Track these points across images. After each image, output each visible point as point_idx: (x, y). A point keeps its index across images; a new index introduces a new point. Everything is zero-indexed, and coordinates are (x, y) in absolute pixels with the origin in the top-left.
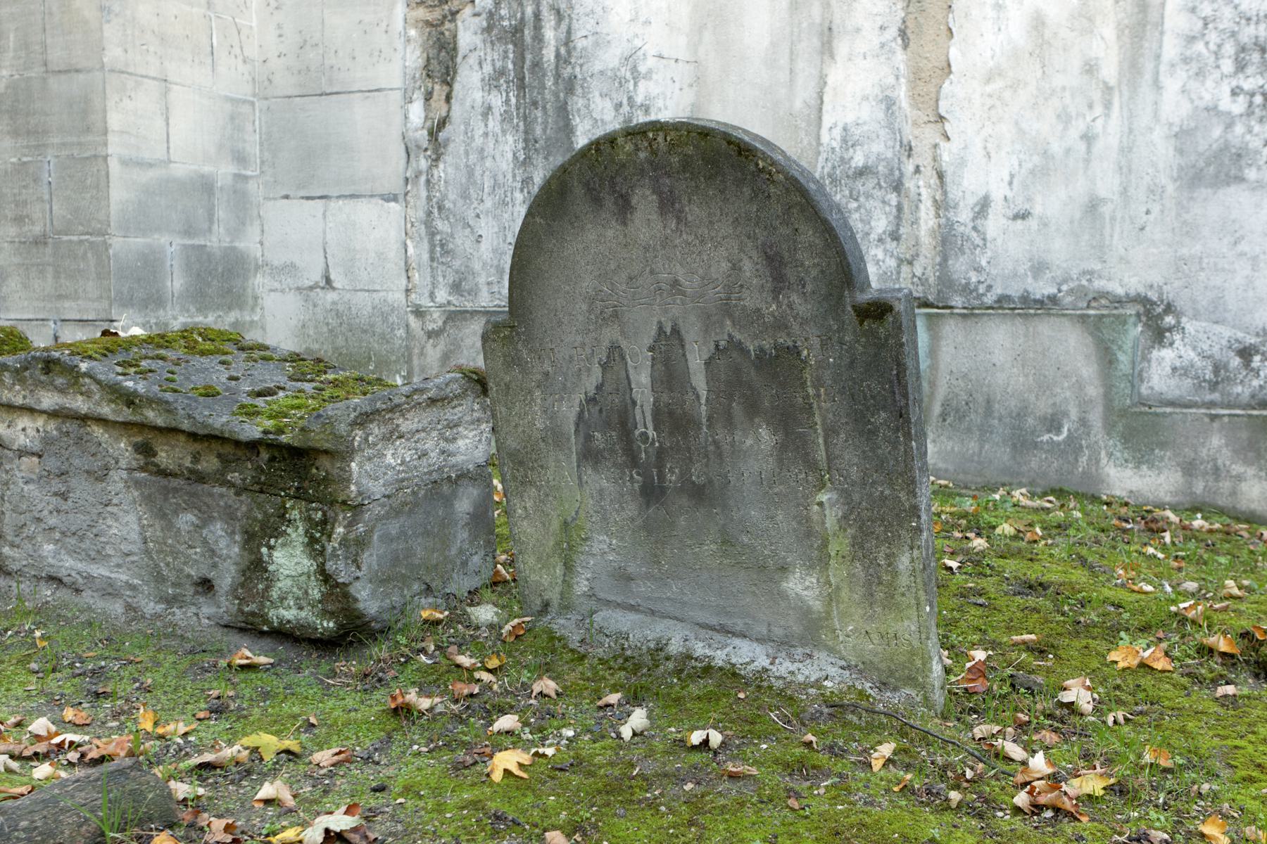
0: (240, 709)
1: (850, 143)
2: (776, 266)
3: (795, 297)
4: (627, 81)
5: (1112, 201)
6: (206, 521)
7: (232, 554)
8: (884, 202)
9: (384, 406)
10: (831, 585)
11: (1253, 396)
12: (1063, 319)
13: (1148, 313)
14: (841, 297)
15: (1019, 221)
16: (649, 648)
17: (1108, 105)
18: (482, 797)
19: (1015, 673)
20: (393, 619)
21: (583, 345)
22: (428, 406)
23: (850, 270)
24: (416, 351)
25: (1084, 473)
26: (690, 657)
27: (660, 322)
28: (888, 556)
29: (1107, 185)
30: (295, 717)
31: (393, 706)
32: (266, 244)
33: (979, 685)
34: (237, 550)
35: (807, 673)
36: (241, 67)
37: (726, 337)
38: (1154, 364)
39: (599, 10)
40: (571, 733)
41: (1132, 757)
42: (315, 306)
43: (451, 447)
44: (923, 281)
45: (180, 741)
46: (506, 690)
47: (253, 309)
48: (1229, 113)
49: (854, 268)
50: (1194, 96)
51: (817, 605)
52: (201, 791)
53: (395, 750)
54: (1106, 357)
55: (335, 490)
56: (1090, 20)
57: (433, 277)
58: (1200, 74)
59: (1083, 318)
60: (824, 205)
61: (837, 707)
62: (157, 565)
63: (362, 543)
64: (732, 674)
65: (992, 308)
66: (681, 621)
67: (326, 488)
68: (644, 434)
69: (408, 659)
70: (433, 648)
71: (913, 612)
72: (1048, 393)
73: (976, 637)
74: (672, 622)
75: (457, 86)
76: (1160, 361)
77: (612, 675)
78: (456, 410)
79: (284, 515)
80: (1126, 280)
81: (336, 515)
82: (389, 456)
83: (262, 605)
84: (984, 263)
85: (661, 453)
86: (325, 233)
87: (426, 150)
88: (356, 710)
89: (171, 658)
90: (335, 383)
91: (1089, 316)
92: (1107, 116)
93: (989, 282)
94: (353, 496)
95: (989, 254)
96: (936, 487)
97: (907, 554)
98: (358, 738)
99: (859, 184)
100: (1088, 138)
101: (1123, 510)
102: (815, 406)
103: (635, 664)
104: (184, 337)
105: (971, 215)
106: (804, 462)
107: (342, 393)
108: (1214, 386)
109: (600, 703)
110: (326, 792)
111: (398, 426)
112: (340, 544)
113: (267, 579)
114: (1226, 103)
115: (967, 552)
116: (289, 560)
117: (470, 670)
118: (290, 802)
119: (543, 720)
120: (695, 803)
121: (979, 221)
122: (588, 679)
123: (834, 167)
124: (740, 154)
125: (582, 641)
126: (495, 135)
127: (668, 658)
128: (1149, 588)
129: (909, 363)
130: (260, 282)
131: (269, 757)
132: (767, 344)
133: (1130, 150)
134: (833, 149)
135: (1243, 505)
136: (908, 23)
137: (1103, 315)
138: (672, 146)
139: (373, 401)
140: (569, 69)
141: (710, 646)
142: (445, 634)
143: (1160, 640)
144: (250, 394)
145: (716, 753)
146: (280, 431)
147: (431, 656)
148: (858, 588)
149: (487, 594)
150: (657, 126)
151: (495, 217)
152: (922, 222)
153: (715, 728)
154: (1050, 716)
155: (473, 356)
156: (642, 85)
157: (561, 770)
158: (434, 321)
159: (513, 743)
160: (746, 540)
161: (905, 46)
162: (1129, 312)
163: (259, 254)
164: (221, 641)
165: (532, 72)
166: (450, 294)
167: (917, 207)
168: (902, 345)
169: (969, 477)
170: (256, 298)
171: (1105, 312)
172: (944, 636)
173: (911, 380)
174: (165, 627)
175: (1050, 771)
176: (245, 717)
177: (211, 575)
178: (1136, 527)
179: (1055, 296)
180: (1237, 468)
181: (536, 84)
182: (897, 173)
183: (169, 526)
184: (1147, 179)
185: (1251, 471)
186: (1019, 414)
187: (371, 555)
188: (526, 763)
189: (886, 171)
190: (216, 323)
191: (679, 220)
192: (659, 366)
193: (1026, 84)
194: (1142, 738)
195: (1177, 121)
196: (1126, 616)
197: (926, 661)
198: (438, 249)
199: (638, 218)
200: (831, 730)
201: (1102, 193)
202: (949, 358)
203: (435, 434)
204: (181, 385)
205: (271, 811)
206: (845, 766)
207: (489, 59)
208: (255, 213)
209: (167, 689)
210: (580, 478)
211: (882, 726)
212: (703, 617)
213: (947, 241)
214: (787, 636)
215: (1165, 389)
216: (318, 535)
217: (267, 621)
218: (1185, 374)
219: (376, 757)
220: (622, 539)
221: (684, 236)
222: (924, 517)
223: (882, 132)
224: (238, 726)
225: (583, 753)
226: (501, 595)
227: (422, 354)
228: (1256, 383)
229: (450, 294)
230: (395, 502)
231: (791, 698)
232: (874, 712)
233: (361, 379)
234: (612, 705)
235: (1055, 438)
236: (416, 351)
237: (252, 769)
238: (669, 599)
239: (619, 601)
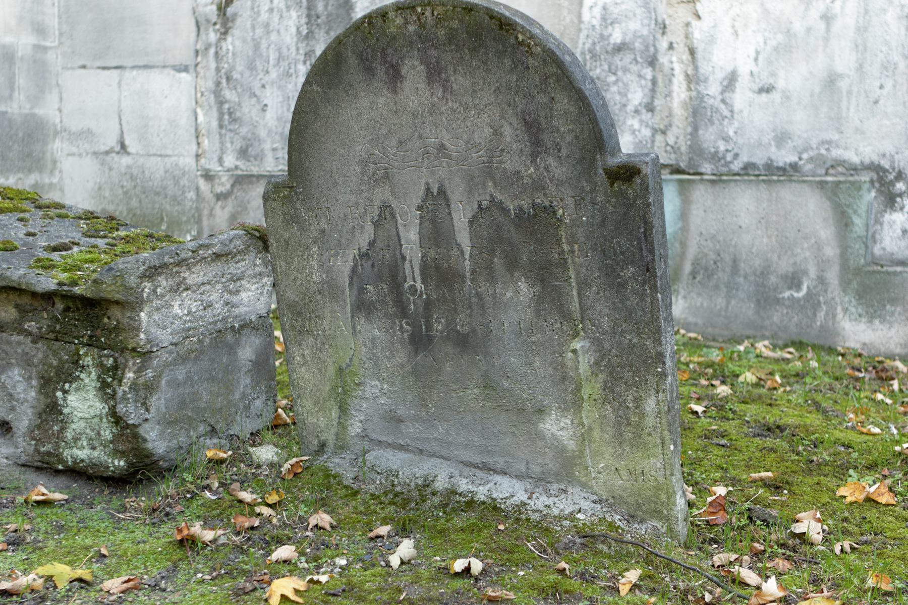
0: (35, 541)
1: (609, 21)
2: (534, 130)
3: (551, 161)
5: (849, 76)
7: (29, 398)
8: (640, 76)
9: (172, 261)
10: (584, 426)
12: (804, 185)
13: (881, 179)
14: (593, 161)
15: (764, 95)
16: (417, 484)
19: (752, 507)
20: (179, 458)
21: (357, 205)
22: (213, 260)
23: (602, 136)
24: (206, 212)
25: (821, 326)
26: (454, 492)
27: (427, 184)
28: (636, 399)
30: (87, 548)
31: (179, 538)
32: (65, 111)
33: (720, 518)
35: (561, 506)
37: (488, 198)
38: (886, 227)
40: (343, 562)
41: (856, 582)
42: (111, 169)
43: (235, 299)
44: (675, 149)
46: (284, 523)
47: (52, 172)
49: (605, 133)
51: (571, 445)
53: (181, 578)
54: (843, 221)
55: (126, 338)
57: (222, 143)
59: (822, 185)
60: (578, 76)
61: (588, 538)
63: (151, 387)
64: (493, 508)
65: (738, 174)
66: (447, 459)
67: (117, 336)
68: (413, 288)
69: (194, 495)
70: (217, 485)
72: (789, 253)
73: (718, 475)
74: (438, 461)
76: (892, 223)
77: (383, 509)
78: (239, 265)
79: (77, 361)
80: (861, 149)
81: (127, 361)
83: (57, 446)
84: (731, 133)
86: (120, 101)
87: (215, 24)
88: (144, 542)
90: (127, 240)
91: (826, 182)
93: (736, 151)
94: (142, 343)
95: (736, 124)
96: (685, 339)
97: (653, 398)
98: (146, 567)
99: (617, 60)
101: (857, 361)
102: (569, 261)
103: (404, 499)
105: (720, 89)
106: (559, 312)
107: (133, 249)
109: (371, 535)
111: (184, 279)
112: (130, 388)
115: (711, 398)
116: (83, 404)
117: (251, 505)
119: (318, 550)
121: (727, 95)
123: (594, 44)
124: (501, 28)
125: (356, 478)
126: (280, 11)
128: (876, 430)
129: (656, 222)
130: (58, 147)
131: (62, 585)
132: (526, 204)
133: (866, 29)
134: (593, 26)
137: (840, 182)
138: (438, 20)
139: (161, 255)
141: (473, 482)
142: (228, 473)
143: (885, 477)
144: (46, 249)
145: (477, 579)
146: (74, 283)
147: (215, 493)
148: (609, 429)
149: (269, 435)
151: (279, 87)
152: (675, 95)
153: (476, 557)
154: (783, 546)
155: (256, 216)
157: (334, 595)
158: (223, 184)
159: (290, 571)
160: (506, 384)
162: (863, 179)
163: (58, 121)
164: (18, 479)
166: (237, 159)
167: (670, 81)
168: (649, 205)
169: (717, 331)
170: (55, 162)
171: (842, 179)
172: (689, 474)
173: (657, 238)
175: (781, 594)
176: (41, 549)
177: (9, 418)
178: (868, 376)
179: (796, 164)
182: (652, 49)
186: (762, 273)
187: (159, 399)
188: (302, 589)
189: (642, 48)
190: (16, 184)
191: (445, 88)
192: (426, 224)
194: (866, 565)
196: (855, 455)
197: (671, 495)
198: (226, 117)
199: (407, 86)
200: (583, 558)
201: (840, 69)
202: (687, 219)
203: (219, 286)
206: (594, 590)
208: (54, 82)
210: (354, 328)
211: (629, 555)
212: (467, 456)
213: (698, 112)
214: (543, 473)
215: (896, 249)
216: (109, 380)
217: (61, 461)
219: (163, 584)
220: (393, 384)
221: (450, 104)
222: (669, 363)
223: (639, 11)
224: (34, 557)
225: (355, 580)
226: (281, 436)
227: (211, 215)
229: (237, 159)
230: (182, 350)
231: (547, 530)
232: (622, 542)
233: (151, 236)
234: (382, 537)
235: (796, 295)
236: (206, 212)
238: (435, 439)
239: (390, 441)
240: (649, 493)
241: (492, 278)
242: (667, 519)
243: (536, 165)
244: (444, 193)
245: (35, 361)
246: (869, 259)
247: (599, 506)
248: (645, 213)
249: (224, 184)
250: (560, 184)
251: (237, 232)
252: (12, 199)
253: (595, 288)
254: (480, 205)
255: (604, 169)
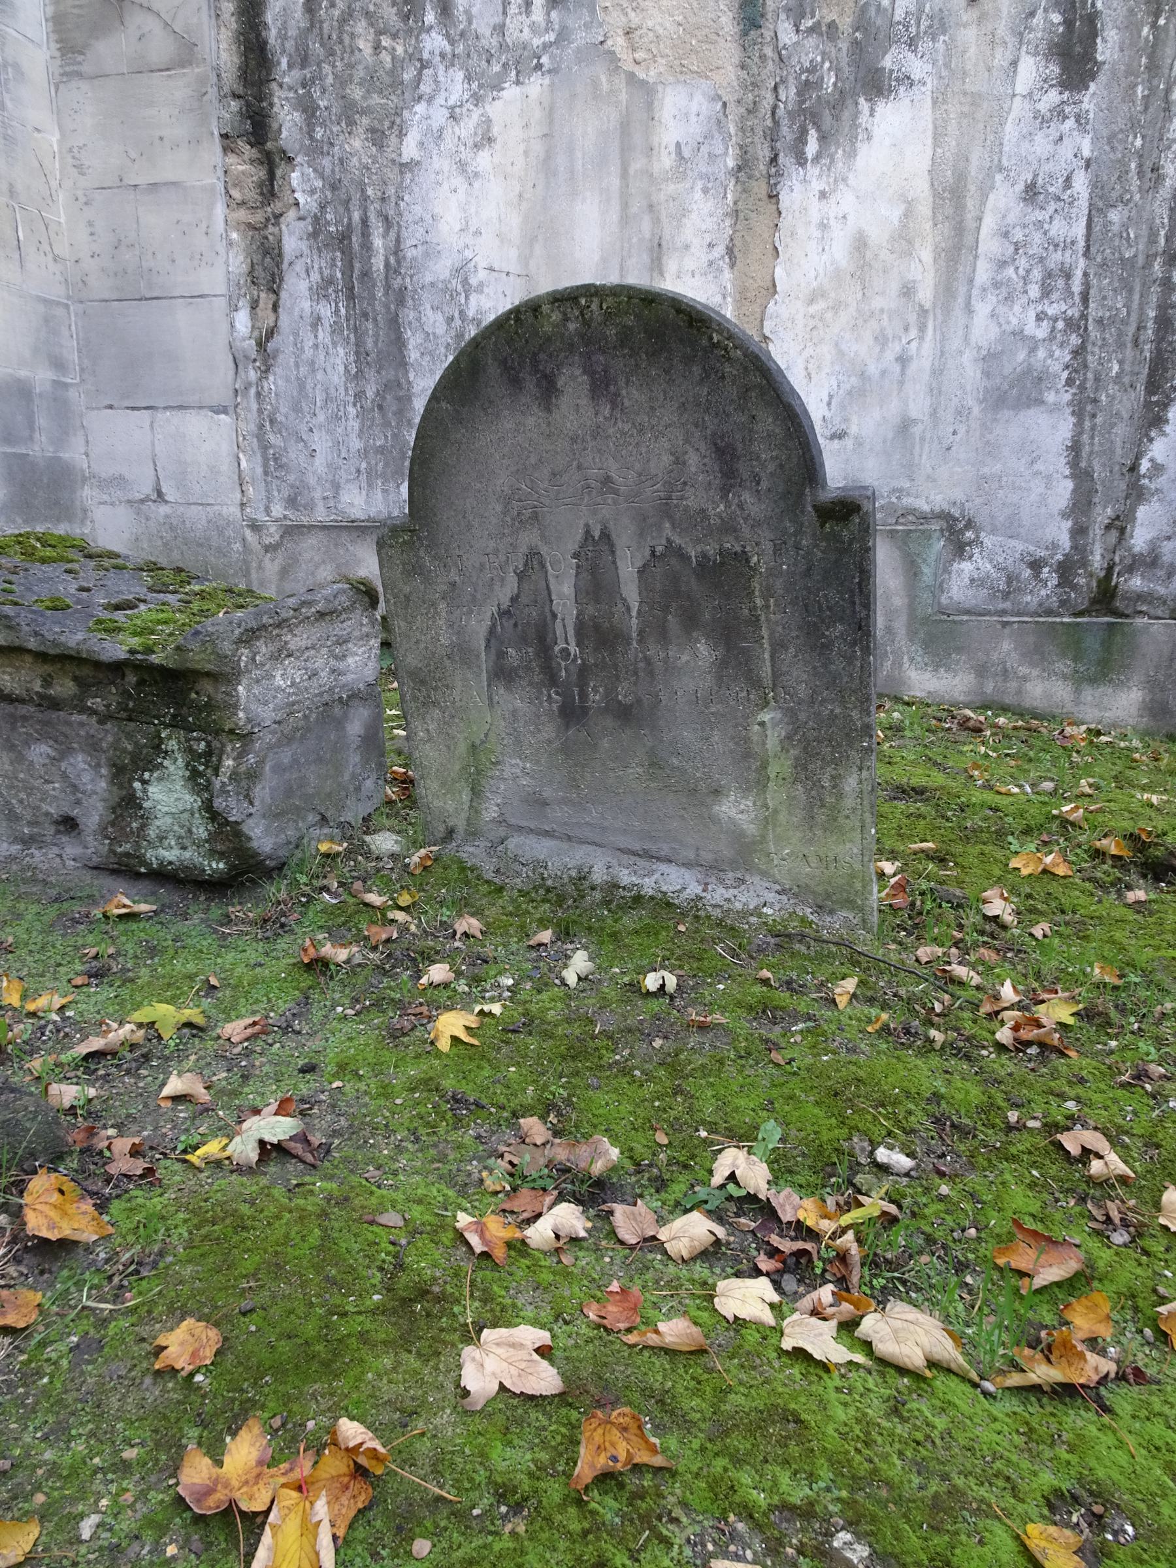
0: (124, 970)
2: (727, 458)
3: (747, 496)
4: (458, 294)
6: (65, 752)
7: (98, 790)
11: (1040, 605)
13: (950, 528)
14: (801, 495)
17: (922, 328)
18: (431, 1074)
21: (496, 552)
22: (317, 620)
24: (254, 565)
25: (888, 676)
26: (616, 886)
27: (587, 525)
29: (918, 407)
30: (191, 977)
32: (92, 454)
34: (104, 784)
36: (53, 267)
37: (664, 542)
38: (954, 576)
39: (428, 217)
40: (510, 982)
43: (341, 665)
45: (55, 1017)
46: (424, 931)
47: (82, 522)
48: (1033, 337)
50: (1002, 320)
51: (751, 829)
52: (92, 1092)
53: (317, 1015)
55: (220, 718)
56: (910, 242)
57: (267, 491)
58: (1009, 299)
61: (783, 938)
62: (8, 803)
63: (253, 776)
64: (664, 904)
67: (209, 715)
68: (565, 651)
71: (857, 835)
75: (284, 295)
79: (159, 746)
80: (932, 497)
81: (223, 745)
82: (278, 678)
85: (584, 671)
86: (153, 445)
88: (261, 965)
89: (34, 909)
90: (202, 595)
91: (897, 531)
92: (922, 338)
97: (855, 776)
100: (903, 360)
102: (763, 618)
103: (558, 895)
104: (20, 543)
108: (1006, 595)
110: (245, 1078)
112: (230, 778)
113: (142, 817)
114: (1031, 328)
116: (168, 796)
117: (382, 910)
118: (204, 1096)
120: (672, 1063)
122: (511, 914)
124: (691, 325)
125: (497, 871)
126: (325, 347)
127: (593, 888)
130: (88, 494)
132: (711, 549)
135: (1027, 703)
136: (736, 242)
138: (608, 316)
139: (258, 615)
140: (399, 279)
146: (149, 650)
147: (335, 895)
150: (590, 291)
151: (328, 431)
156: (473, 298)
157: (514, 1031)
158: (271, 535)
161: (732, 265)
163: (85, 466)
164: (91, 886)
165: (362, 282)
166: (286, 508)
170: (85, 511)
174: (23, 870)
175: (1017, 999)
176: (132, 981)
177: (74, 813)
180: (1023, 670)
181: (365, 294)
183: (20, 758)
184: (955, 400)
185: (1035, 672)
192: (584, 575)
193: (847, 305)
195: (985, 344)
199: (565, 403)
201: (914, 414)
203: (324, 651)
204: (22, 597)
205: (183, 1112)
207: (316, 266)
209: (32, 947)
210: (490, 698)
216: (202, 768)
217: (143, 862)
218: (982, 585)
220: (537, 762)
221: (620, 425)
224: (125, 992)
227: (260, 567)
228: (1043, 592)
229: (286, 508)
231: (732, 929)
236: (254, 565)
237: (147, 1054)
240: (841, 881)
241: (664, 637)
242: (861, 909)
243: (727, 501)
244: (608, 537)
245: (104, 745)
246: (936, 608)
247: (784, 898)
248: (862, 559)
249: (273, 535)
250: (757, 524)
251: (340, 585)
252: (54, 547)
253: (792, 650)
254: (653, 552)
255: (814, 507)
